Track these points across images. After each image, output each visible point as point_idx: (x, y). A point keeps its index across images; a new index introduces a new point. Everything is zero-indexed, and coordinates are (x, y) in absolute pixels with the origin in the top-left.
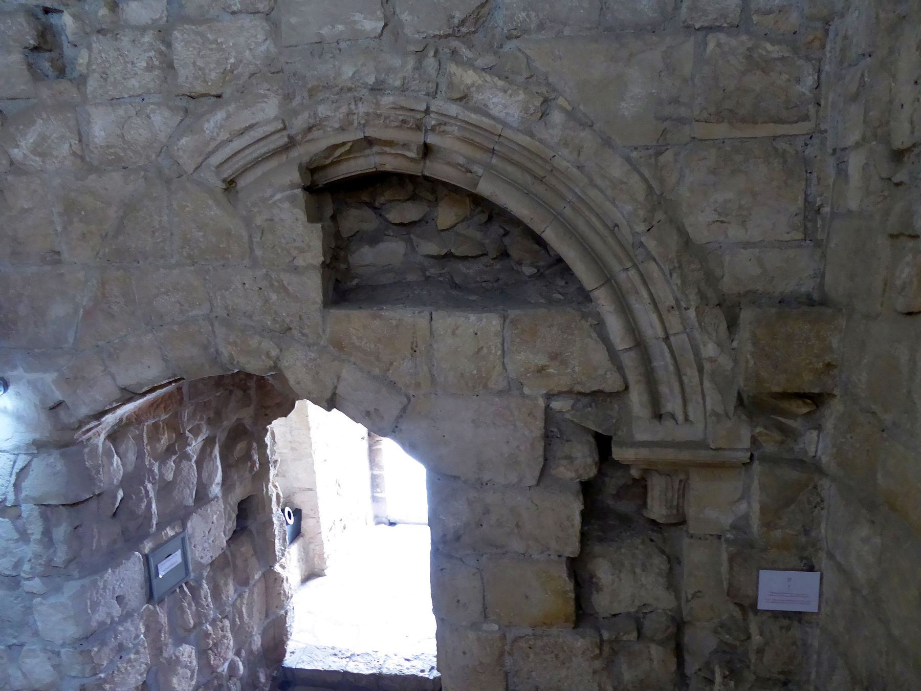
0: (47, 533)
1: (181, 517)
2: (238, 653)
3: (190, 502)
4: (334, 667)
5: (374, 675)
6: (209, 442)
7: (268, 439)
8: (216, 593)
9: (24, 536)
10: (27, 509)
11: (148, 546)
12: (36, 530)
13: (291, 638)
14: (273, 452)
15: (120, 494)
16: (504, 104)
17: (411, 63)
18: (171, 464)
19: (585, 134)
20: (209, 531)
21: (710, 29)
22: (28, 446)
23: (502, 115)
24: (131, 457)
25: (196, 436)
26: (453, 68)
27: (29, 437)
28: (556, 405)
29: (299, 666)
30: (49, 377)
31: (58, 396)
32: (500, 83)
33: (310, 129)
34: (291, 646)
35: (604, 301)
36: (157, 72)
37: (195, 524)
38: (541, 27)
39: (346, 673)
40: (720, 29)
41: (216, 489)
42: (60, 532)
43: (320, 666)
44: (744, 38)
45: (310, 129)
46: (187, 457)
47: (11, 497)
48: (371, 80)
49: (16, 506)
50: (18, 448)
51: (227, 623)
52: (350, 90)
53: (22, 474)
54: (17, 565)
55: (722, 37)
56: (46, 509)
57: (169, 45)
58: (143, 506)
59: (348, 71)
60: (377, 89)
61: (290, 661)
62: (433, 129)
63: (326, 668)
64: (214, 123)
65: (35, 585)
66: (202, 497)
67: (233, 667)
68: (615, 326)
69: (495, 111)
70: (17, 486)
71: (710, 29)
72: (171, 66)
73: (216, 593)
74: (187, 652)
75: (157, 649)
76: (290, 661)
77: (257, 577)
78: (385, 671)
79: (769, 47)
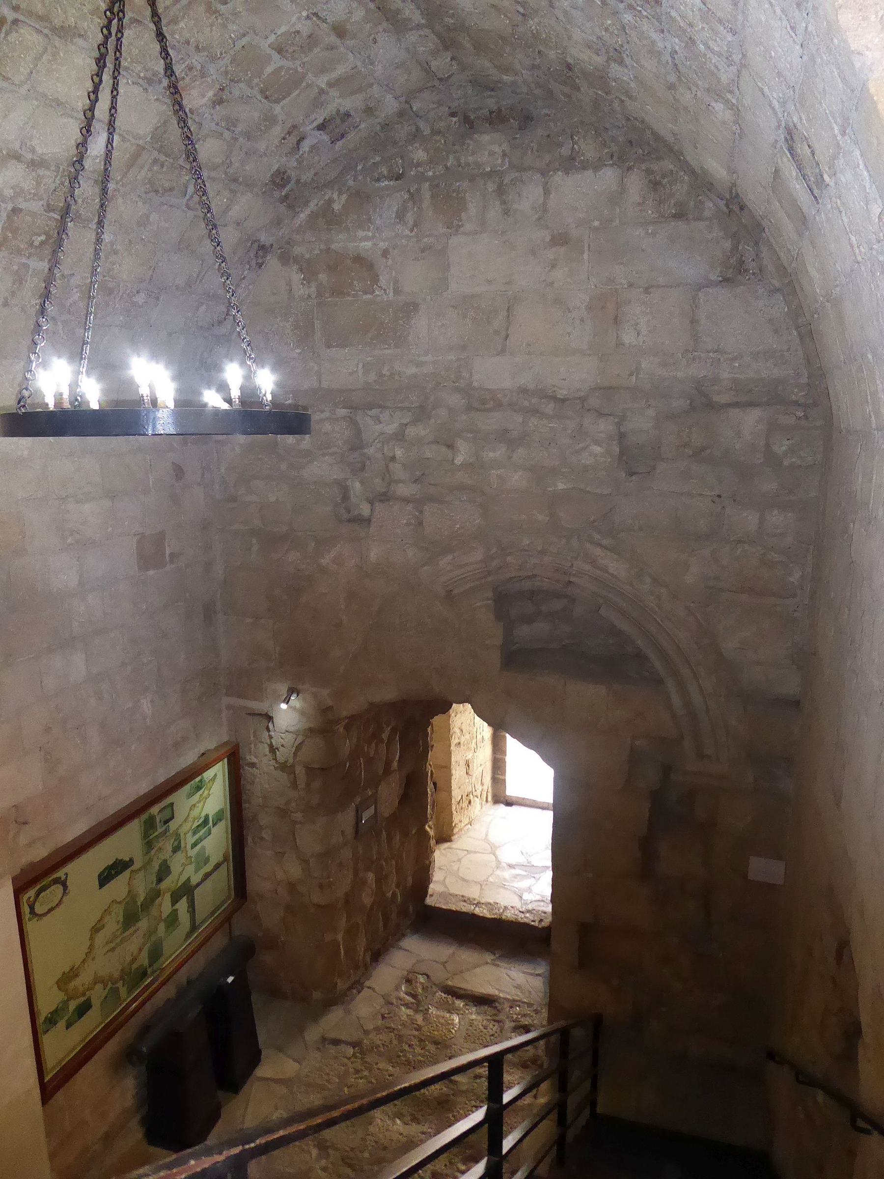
0: (308, 784)
1: (375, 782)
2: (398, 886)
3: (381, 772)
4: (464, 910)
5: (495, 919)
6: (394, 730)
7: (429, 729)
8: (390, 839)
9: (294, 785)
10: (300, 771)
11: (358, 799)
12: (302, 784)
13: (434, 879)
14: (432, 739)
15: (348, 765)
16: (616, 567)
17: (564, 541)
18: (374, 745)
19: (663, 590)
20: (389, 793)
21: (739, 542)
22: (305, 730)
23: (615, 573)
24: (355, 741)
25: (388, 726)
26: (588, 545)
27: (308, 725)
28: (637, 743)
29: (437, 905)
30: (325, 692)
31: (329, 703)
32: (616, 557)
33: (500, 568)
34: (433, 887)
35: (671, 685)
36: (412, 527)
37: (383, 789)
38: (641, 529)
39: (474, 916)
40: (744, 542)
41: (395, 765)
42: (316, 785)
43: (454, 908)
44: (759, 548)
45: (500, 568)
46: (382, 741)
47: (291, 761)
48: (539, 548)
49: (293, 766)
50: (298, 731)
51: (394, 862)
52: (526, 551)
53: (298, 748)
54: (288, 803)
55: (746, 547)
56: (309, 770)
57: (421, 512)
58: (358, 773)
59: (526, 542)
60: (543, 552)
61: (429, 901)
62: (574, 575)
63: (458, 909)
64: (445, 561)
65: (298, 816)
66: (387, 770)
67: (394, 894)
68: (676, 700)
69: (611, 571)
70: (295, 754)
71: (739, 542)
72: (420, 523)
73: (390, 839)
74: (371, 876)
75: (356, 873)
76: (429, 901)
77: (414, 832)
78: (504, 917)
79: (773, 554)
